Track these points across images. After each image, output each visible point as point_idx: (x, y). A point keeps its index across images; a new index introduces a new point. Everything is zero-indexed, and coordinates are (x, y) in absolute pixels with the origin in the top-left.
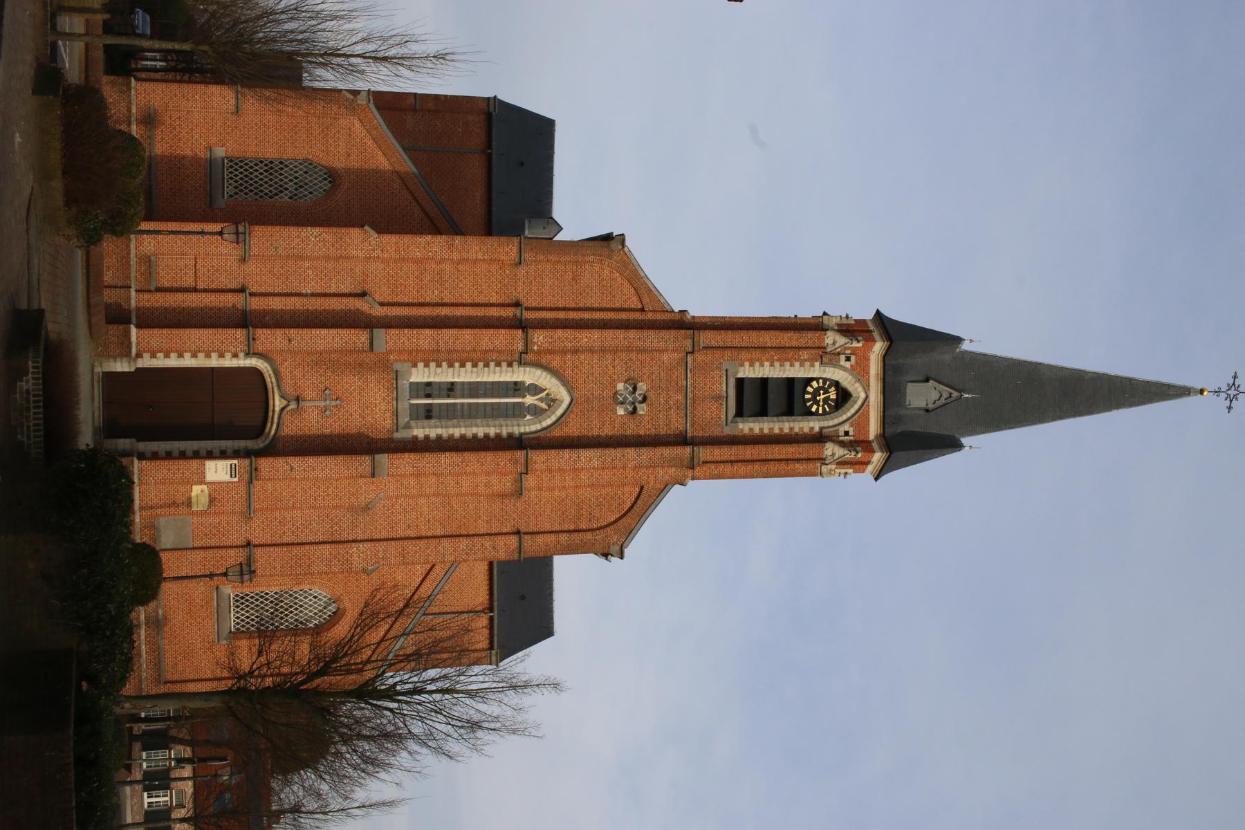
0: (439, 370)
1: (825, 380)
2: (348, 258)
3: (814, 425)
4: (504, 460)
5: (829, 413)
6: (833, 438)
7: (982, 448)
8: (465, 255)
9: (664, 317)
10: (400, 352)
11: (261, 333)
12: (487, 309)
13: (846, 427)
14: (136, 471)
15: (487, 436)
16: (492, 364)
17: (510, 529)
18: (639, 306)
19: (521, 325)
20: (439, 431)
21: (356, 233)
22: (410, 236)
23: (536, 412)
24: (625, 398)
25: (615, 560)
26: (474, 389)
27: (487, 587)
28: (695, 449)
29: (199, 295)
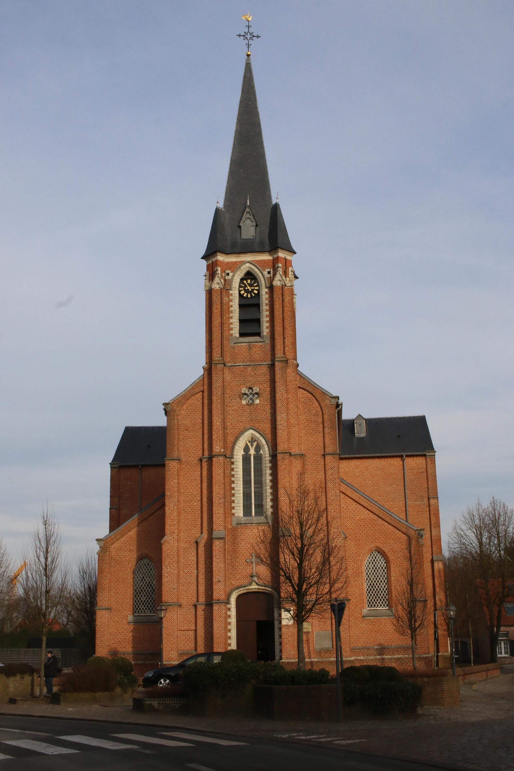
0: (236, 501)
1: (240, 287)
2: (178, 551)
3: (264, 291)
4: (282, 466)
5: (258, 283)
6: (272, 280)
7: (279, 192)
8: (175, 489)
9: (206, 379)
10: (225, 522)
11: (215, 596)
12: (203, 476)
13: (265, 273)
14: (287, 661)
15: (271, 475)
16: (233, 473)
17: (322, 460)
18: (201, 393)
19: (210, 459)
20: (268, 500)
21: (165, 547)
22: (166, 519)
23: (258, 448)
24: (251, 399)
25: (340, 401)
26: (247, 482)
27: (389, 459)
28: (279, 360)
29: (198, 628)
